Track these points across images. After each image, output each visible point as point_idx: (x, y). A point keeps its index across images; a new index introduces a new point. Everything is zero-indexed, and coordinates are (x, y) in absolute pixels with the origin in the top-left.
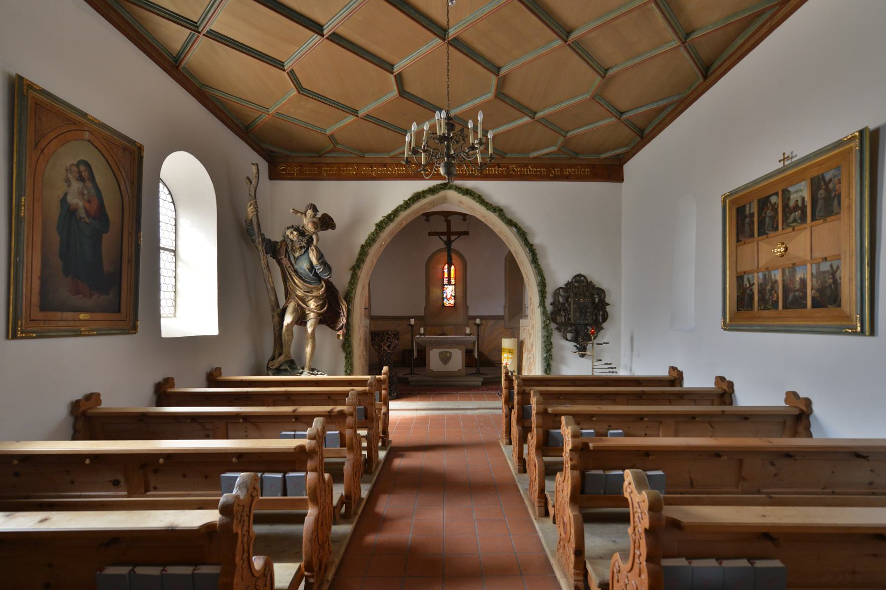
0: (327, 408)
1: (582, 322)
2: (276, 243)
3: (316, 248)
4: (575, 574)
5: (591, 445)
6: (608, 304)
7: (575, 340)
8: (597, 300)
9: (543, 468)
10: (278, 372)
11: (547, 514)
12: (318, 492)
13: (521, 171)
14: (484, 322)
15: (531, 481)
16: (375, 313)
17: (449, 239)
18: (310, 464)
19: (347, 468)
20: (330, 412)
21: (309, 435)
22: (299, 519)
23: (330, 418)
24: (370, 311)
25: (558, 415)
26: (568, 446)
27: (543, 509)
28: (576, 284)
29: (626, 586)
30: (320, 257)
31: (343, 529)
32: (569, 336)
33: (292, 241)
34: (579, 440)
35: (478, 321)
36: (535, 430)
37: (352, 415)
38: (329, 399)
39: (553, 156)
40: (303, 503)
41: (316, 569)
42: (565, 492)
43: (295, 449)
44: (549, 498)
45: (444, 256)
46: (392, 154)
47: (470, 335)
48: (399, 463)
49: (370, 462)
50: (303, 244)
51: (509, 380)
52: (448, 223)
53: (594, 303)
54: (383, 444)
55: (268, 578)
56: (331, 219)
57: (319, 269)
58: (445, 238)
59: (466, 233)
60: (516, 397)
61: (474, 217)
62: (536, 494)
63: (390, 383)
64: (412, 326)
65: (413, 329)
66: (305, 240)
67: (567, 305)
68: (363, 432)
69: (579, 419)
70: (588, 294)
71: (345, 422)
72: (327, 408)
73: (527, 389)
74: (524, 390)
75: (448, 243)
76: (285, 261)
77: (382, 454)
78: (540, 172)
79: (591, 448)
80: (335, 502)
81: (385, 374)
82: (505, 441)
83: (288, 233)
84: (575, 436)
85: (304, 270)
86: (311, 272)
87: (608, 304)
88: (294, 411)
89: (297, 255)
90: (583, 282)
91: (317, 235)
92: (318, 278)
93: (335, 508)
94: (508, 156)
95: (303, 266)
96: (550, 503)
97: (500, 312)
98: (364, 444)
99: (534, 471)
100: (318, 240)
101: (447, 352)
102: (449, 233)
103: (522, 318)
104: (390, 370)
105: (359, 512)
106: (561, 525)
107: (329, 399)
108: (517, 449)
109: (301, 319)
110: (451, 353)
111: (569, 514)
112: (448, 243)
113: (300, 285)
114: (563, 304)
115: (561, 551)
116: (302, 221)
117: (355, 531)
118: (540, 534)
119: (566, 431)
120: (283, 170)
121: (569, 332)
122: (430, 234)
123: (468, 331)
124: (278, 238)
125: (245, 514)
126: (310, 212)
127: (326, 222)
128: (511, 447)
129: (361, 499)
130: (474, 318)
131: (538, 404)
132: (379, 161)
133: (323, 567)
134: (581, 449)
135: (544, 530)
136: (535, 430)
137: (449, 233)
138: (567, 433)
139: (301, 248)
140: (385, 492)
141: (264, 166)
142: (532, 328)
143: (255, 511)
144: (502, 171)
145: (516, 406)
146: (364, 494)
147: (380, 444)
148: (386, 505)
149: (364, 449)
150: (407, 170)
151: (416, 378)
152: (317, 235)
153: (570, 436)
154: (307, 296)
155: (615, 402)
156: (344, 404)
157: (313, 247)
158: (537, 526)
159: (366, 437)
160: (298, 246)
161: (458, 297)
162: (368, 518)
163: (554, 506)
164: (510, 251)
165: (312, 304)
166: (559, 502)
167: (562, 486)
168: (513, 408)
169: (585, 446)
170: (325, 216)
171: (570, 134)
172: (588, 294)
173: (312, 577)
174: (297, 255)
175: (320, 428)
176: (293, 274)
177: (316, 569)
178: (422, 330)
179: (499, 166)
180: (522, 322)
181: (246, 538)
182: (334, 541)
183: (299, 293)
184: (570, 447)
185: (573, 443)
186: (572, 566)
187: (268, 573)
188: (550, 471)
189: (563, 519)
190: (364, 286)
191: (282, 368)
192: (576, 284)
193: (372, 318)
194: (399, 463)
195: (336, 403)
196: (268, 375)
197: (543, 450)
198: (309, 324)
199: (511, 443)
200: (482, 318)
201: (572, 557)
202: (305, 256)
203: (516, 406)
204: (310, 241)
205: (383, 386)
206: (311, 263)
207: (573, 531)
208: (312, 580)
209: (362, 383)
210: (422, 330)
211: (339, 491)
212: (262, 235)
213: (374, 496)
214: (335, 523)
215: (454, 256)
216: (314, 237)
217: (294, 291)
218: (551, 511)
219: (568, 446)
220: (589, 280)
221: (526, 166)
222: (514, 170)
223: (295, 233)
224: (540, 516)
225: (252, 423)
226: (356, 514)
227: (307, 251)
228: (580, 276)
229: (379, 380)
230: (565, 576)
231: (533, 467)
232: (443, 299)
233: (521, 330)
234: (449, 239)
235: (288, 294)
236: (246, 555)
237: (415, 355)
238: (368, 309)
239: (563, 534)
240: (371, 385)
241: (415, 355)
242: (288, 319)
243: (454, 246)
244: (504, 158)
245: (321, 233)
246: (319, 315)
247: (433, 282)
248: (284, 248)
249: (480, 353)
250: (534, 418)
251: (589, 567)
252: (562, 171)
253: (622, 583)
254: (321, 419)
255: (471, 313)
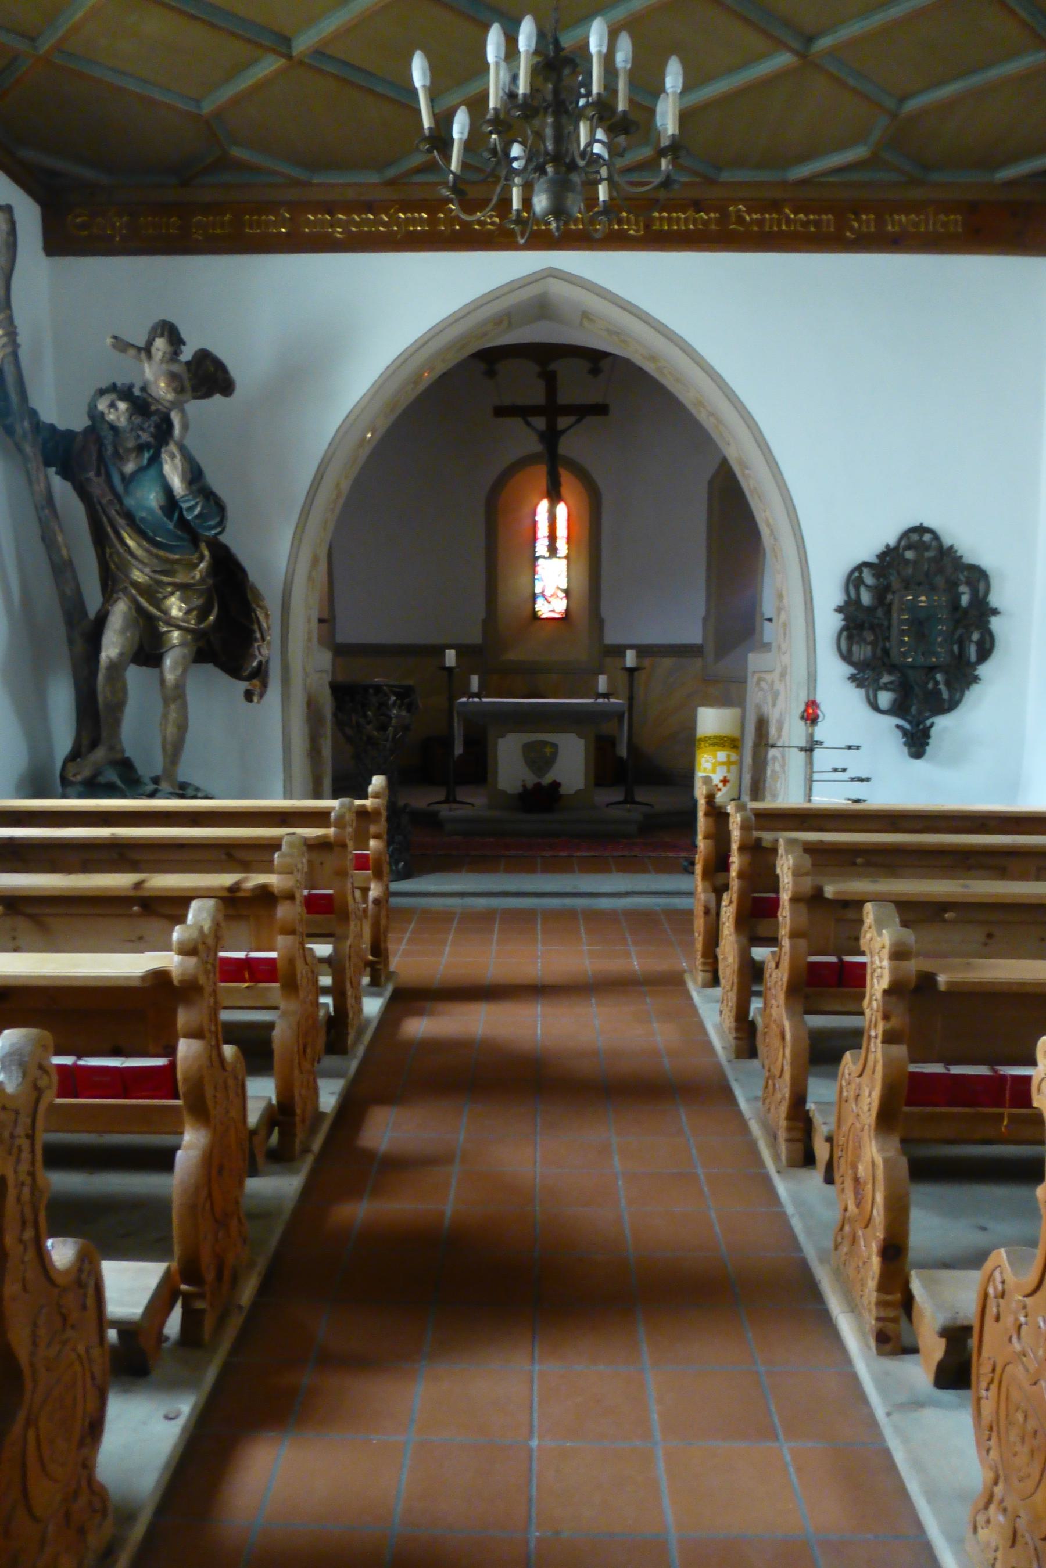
0: (227, 879)
1: (921, 660)
2: (70, 434)
3: (182, 448)
4: (879, 1304)
5: (942, 979)
6: (995, 612)
7: (898, 709)
8: (965, 600)
9: (806, 1043)
10: (93, 788)
11: (808, 1160)
12: (209, 1092)
13: (760, 223)
14: (647, 662)
15: (771, 1077)
16: (343, 637)
17: (552, 426)
18: (184, 1018)
19: (281, 1035)
20: (234, 889)
21: (181, 943)
22: (162, 1160)
23: (233, 903)
24: (332, 633)
25: (857, 904)
26: (879, 980)
27: (800, 1146)
28: (909, 555)
29: (1020, 1326)
30: (195, 475)
31: (276, 1187)
32: (885, 698)
33: (113, 428)
34: (912, 966)
35: (630, 659)
36: (786, 943)
37: (290, 897)
38: (228, 855)
39: (855, 176)
40: (174, 1124)
41: (210, 1276)
42: (865, 1101)
43: (143, 978)
44: (818, 1119)
45: (539, 474)
46: (391, 173)
47: (605, 696)
48: (418, 1027)
49: (336, 1031)
50: (145, 437)
51: (719, 816)
52: (550, 380)
53: (955, 606)
54: (375, 982)
55: (91, 1291)
56: (220, 366)
57: (193, 509)
58: (540, 423)
59: (601, 410)
60: (735, 861)
61: (627, 363)
62: (784, 1109)
63: (389, 819)
64: (450, 670)
65: (452, 682)
66: (150, 425)
67: (880, 613)
68: (323, 949)
69: (913, 912)
70: (940, 581)
71: (272, 916)
72: (227, 879)
73: (767, 837)
74: (759, 840)
75: (551, 438)
76: (97, 487)
77: (372, 1006)
78: (817, 224)
79: (942, 987)
80: (253, 1118)
81: (376, 796)
82: (700, 976)
83: (102, 405)
84: (898, 954)
85: (150, 511)
86: (170, 517)
87: (995, 612)
88: (138, 885)
89: (130, 467)
90: (927, 547)
91: (183, 412)
92: (190, 533)
93: (253, 1133)
94: (726, 176)
95: (149, 499)
96: (822, 1128)
97: (692, 634)
98: (326, 981)
99: (781, 1048)
100: (185, 426)
101: (545, 743)
102: (551, 409)
103: (751, 650)
104: (391, 784)
105: (317, 1145)
106: (849, 1184)
107: (228, 855)
108: (733, 996)
109: (148, 651)
110: (555, 746)
111: (873, 1155)
112: (551, 438)
113: (139, 552)
114: (870, 610)
115: (845, 1248)
116: (143, 372)
117: (307, 1191)
118: (790, 1209)
119: (878, 946)
120: (83, 226)
121: (885, 687)
122: (501, 411)
123: (602, 683)
124: (78, 423)
125: (20, 1131)
126: (160, 344)
127: (209, 377)
128: (717, 992)
129: (320, 1116)
130: (619, 651)
131: (797, 874)
132: (350, 194)
133: (227, 1274)
134: (914, 992)
135: (803, 1201)
136: (786, 943)
137: (551, 409)
138: (877, 945)
139: (141, 448)
140: (388, 1098)
141: (28, 215)
142: (783, 675)
143: (43, 1137)
144: (706, 223)
145: (735, 884)
146: (328, 1096)
147: (366, 980)
148: (387, 1130)
149: (325, 991)
150: (432, 221)
151: (460, 812)
152: (183, 412)
153: (885, 954)
154: (159, 583)
155: (1003, 873)
156: (271, 871)
157: (172, 447)
158: (782, 1188)
159: (327, 961)
160: (131, 444)
161: (575, 593)
162: (342, 1158)
163: (829, 1139)
164: (724, 464)
165: (175, 607)
166: (845, 1129)
167: (855, 1092)
168: (726, 887)
169: (927, 980)
170: (204, 356)
171: (912, 105)
172: (940, 581)
173: (201, 1296)
174: (130, 467)
175: (207, 926)
176: (121, 522)
177: (210, 1276)
178: (475, 681)
179: (698, 205)
180: (755, 660)
181: (26, 1191)
182: (252, 1216)
183: (138, 576)
184: (885, 984)
185: (893, 971)
186: (872, 1284)
187: (87, 1285)
188: (824, 1053)
189: (854, 1167)
190: (315, 561)
191: (102, 779)
192: (909, 555)
193: (341, 651)
194: (418, 1027)
195: (246, 867)
196: (64, 796)
197: (807, 997)
198: (168, 662)
199: (715, 981)
200: (643, 651)
201: (875, 1262)
202: (152, 472)
203: (735, 884)
204: (164, 431)
205: (373, 829)
206: (168, 491)
207: (880, 1198)
208: (200, 1305)
209: (320, 818)
210: (475, 681)
211: (261, 1091)
212: (34, 413)
213: (352, 1110)
214: (254, 1172)
215: (566, 478)
216: (176, 418)
217: (124, 568)
218: (822, 1151)
219: (879, 980)
220: (947, 541)
221: (775, 206)
222: (740, 220)
223: (122, 406)
224: (793, 1164)
225: (31, 917)
226: (306, 1150)
227: (155, 460)
228: (921, 530)
229: (363, 814)
230: (853, 1308)
231: (776, 1042)
232: (534, 597)
233: (752, 681)
234: (552, 426)
235: (111, 581)
236: (29, 1234)
237: (458, 750)
238: (327, 621)
239: (851, 1206)
240: (340, 823)
241: (458, 750)
242: (112, 646)
243: (566, 447)
244: (711, 182)
245: (195, 407)
246: (198, 635)
247: (500, 550)
248: (93, 449)
249: (632, 747)
250: (785, 913)
251: (916, 1287)
252: (880, 222)
253: (1008, 1321)
254: (210, 903)
255: (612, 637)
